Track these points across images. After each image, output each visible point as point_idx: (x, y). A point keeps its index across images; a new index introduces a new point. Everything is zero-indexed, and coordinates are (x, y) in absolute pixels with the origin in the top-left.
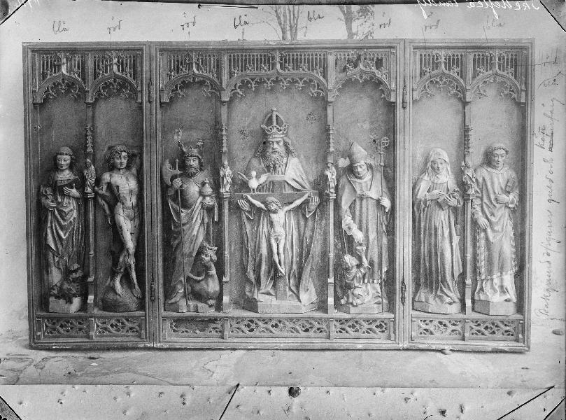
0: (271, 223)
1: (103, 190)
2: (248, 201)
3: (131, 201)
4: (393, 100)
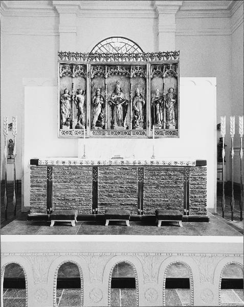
0: (117, 108)
1: (76, 99)
3: (83, 102)
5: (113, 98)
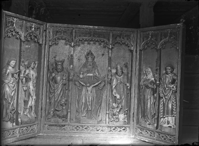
2: (79, 82)
4: (132, 49)
5: (81, 76)
